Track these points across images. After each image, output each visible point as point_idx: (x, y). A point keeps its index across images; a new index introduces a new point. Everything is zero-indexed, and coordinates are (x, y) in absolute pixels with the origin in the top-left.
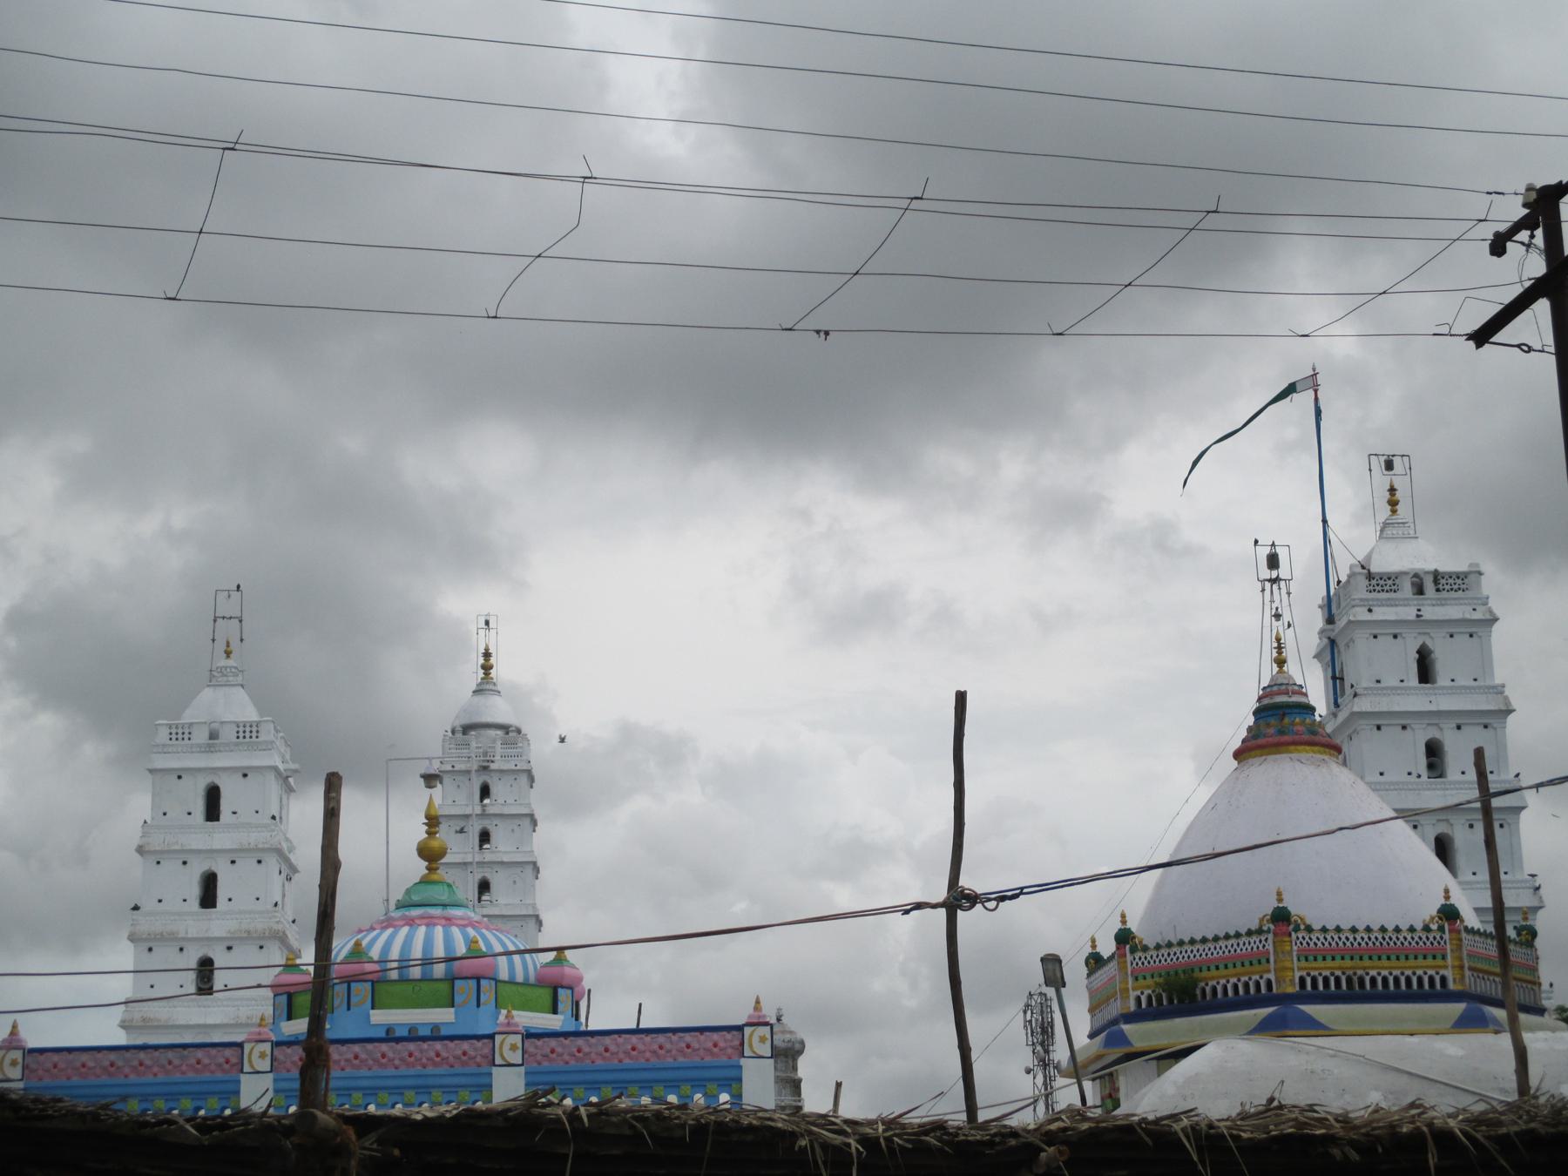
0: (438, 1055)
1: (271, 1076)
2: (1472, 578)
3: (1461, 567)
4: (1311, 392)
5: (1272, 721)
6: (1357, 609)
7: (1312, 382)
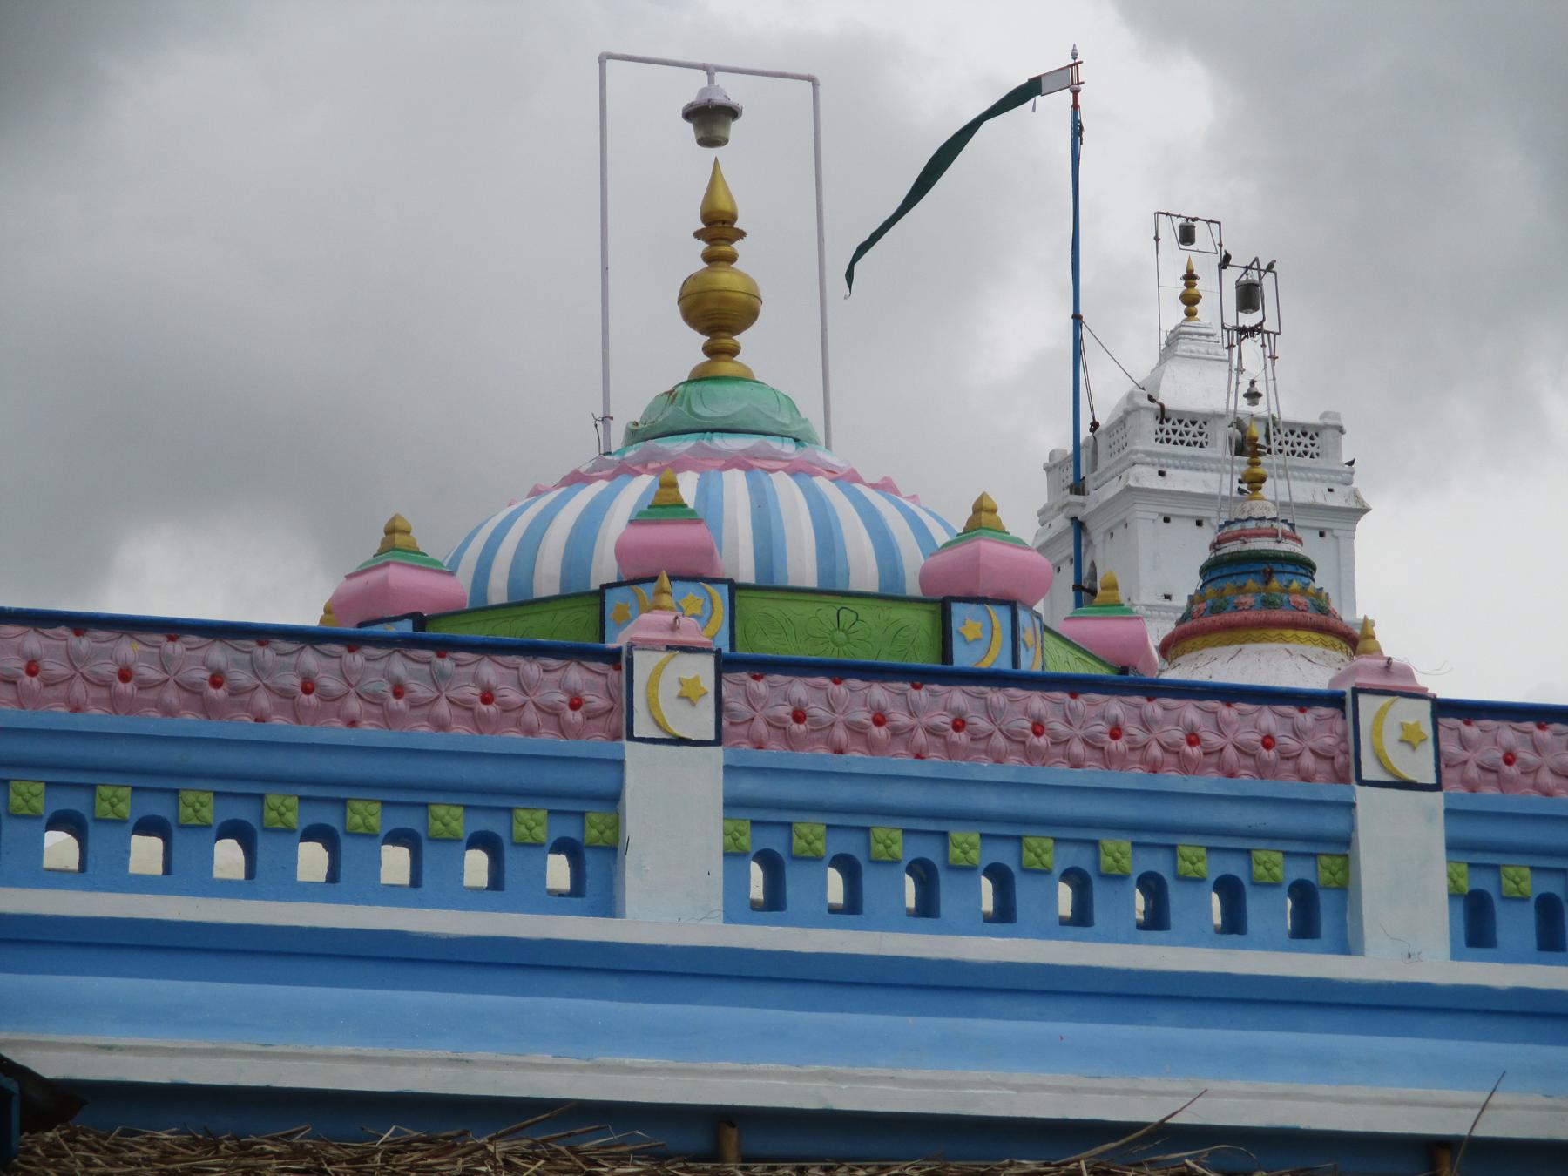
0: (1193, 740)
1: (717, 754)
2: (1327, 436)
3: (1310, 417)
4: (1067, 95)
5: (1251, 583)
6: (1138, 469)
7: (1069, 78)
